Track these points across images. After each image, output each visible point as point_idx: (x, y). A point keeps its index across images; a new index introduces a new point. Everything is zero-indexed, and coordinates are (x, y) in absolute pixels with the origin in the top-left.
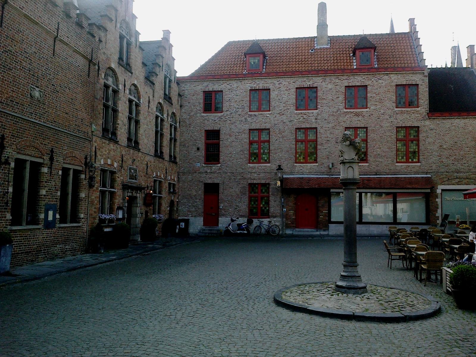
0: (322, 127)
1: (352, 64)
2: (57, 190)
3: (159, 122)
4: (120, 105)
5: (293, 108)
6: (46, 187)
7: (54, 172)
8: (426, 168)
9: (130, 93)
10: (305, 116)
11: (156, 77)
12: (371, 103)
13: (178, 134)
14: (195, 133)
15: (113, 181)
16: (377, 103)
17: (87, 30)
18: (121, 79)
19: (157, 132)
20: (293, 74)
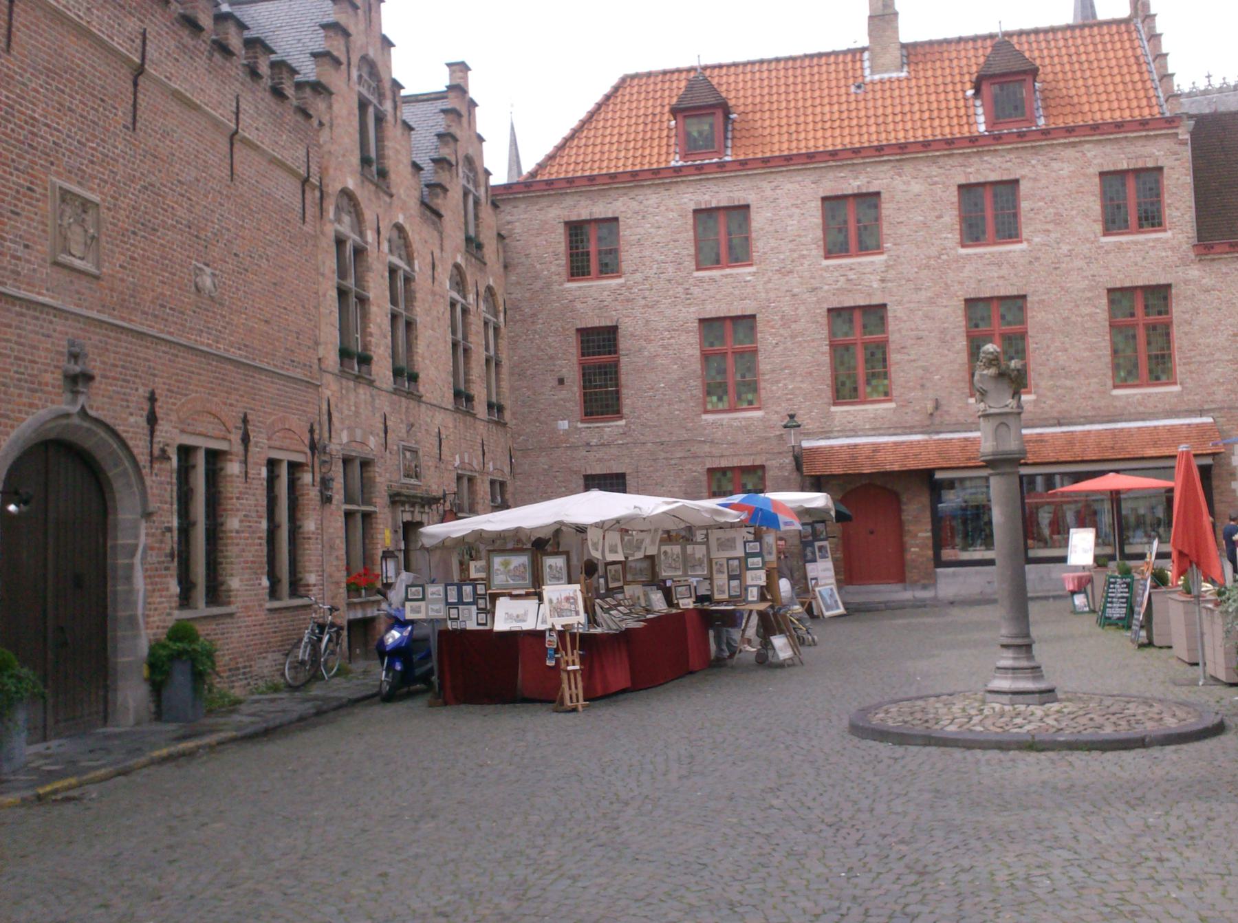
1: (972, 120)
2: (261, 517)
3: (459, 314)
4: (371, 285)
5: (817, 252)
6: (238, 510)
7: (252, 472)
8: (1196, 398)
9: (391, 251)
10: (852, 275)
11: (445, 198)
12: (1031, 228)
13: (503, 343)
14: (550, 339)
15: (367, 485)
16: (1050, 227)
17: (295, 102)
18: (369, 215)
19: (455, 345)
20: (810, 159)
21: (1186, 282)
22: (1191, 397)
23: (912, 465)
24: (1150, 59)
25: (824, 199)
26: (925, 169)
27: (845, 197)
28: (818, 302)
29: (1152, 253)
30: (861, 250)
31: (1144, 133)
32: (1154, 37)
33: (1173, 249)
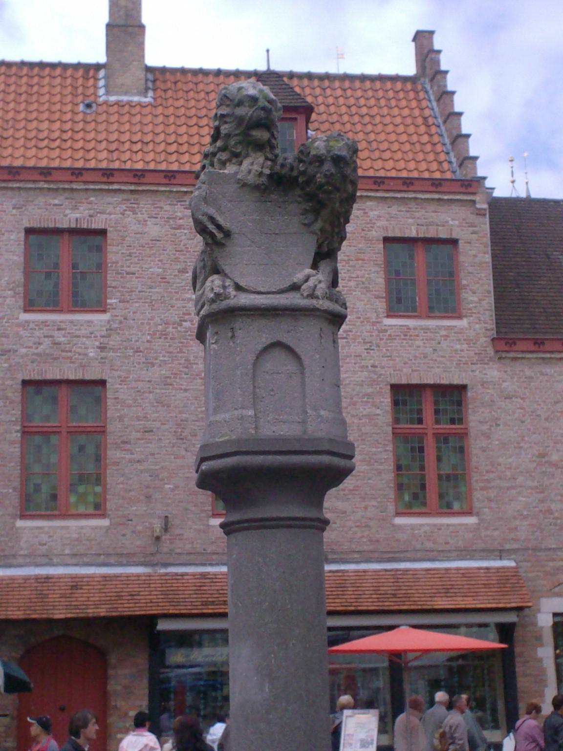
0: (123, 380)
8: (496, 533)
21: (484, 384)
22: (489, 532)
23: (126, 608)
24: (440, 121)
25: (29, 231)
26: (167, 207)
27: (58, 232)
28: (9, 369)
29: (444, 344)
30: (75, 304)
31: (436, 196)
32: (446, 96)
33: (468, 341)
